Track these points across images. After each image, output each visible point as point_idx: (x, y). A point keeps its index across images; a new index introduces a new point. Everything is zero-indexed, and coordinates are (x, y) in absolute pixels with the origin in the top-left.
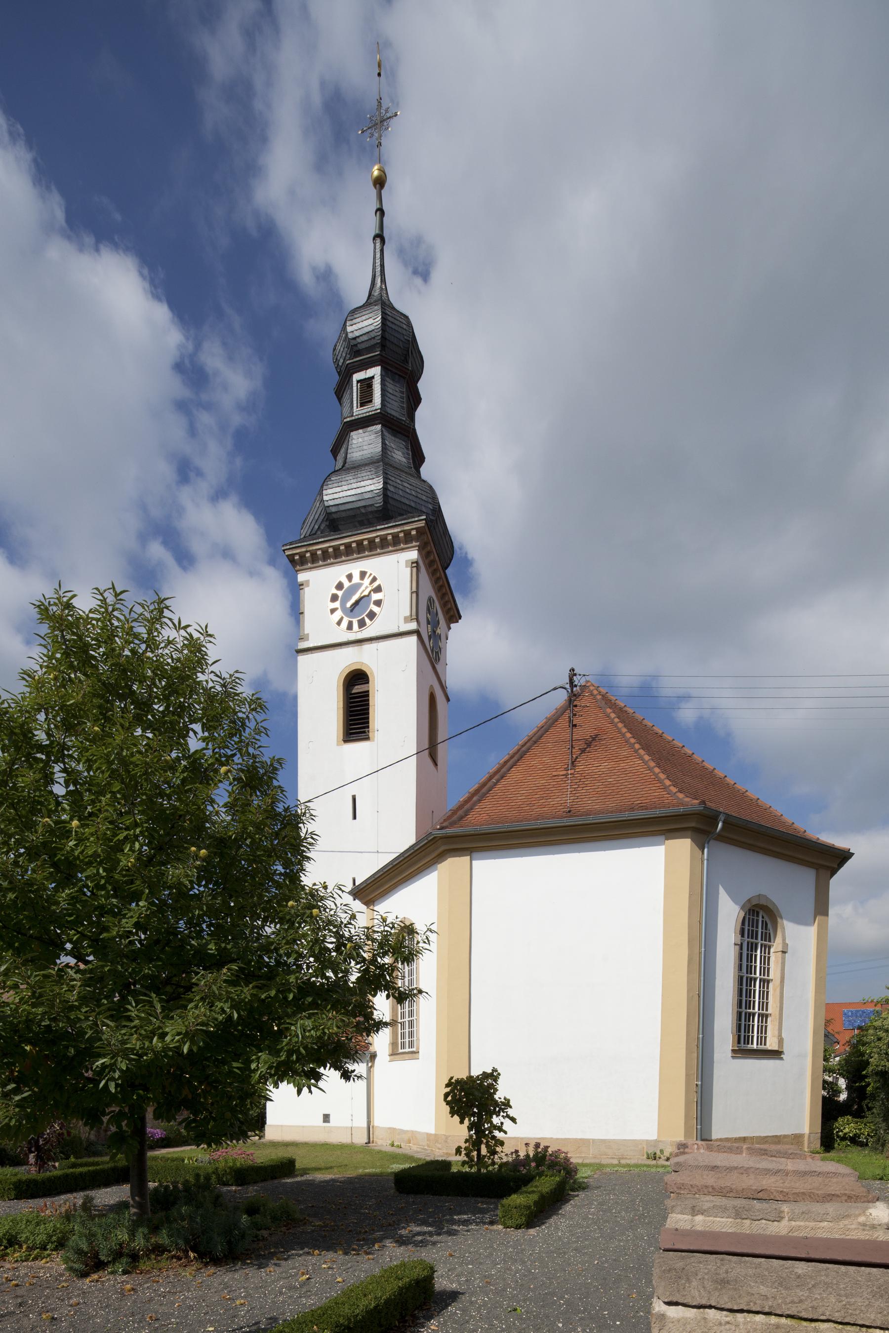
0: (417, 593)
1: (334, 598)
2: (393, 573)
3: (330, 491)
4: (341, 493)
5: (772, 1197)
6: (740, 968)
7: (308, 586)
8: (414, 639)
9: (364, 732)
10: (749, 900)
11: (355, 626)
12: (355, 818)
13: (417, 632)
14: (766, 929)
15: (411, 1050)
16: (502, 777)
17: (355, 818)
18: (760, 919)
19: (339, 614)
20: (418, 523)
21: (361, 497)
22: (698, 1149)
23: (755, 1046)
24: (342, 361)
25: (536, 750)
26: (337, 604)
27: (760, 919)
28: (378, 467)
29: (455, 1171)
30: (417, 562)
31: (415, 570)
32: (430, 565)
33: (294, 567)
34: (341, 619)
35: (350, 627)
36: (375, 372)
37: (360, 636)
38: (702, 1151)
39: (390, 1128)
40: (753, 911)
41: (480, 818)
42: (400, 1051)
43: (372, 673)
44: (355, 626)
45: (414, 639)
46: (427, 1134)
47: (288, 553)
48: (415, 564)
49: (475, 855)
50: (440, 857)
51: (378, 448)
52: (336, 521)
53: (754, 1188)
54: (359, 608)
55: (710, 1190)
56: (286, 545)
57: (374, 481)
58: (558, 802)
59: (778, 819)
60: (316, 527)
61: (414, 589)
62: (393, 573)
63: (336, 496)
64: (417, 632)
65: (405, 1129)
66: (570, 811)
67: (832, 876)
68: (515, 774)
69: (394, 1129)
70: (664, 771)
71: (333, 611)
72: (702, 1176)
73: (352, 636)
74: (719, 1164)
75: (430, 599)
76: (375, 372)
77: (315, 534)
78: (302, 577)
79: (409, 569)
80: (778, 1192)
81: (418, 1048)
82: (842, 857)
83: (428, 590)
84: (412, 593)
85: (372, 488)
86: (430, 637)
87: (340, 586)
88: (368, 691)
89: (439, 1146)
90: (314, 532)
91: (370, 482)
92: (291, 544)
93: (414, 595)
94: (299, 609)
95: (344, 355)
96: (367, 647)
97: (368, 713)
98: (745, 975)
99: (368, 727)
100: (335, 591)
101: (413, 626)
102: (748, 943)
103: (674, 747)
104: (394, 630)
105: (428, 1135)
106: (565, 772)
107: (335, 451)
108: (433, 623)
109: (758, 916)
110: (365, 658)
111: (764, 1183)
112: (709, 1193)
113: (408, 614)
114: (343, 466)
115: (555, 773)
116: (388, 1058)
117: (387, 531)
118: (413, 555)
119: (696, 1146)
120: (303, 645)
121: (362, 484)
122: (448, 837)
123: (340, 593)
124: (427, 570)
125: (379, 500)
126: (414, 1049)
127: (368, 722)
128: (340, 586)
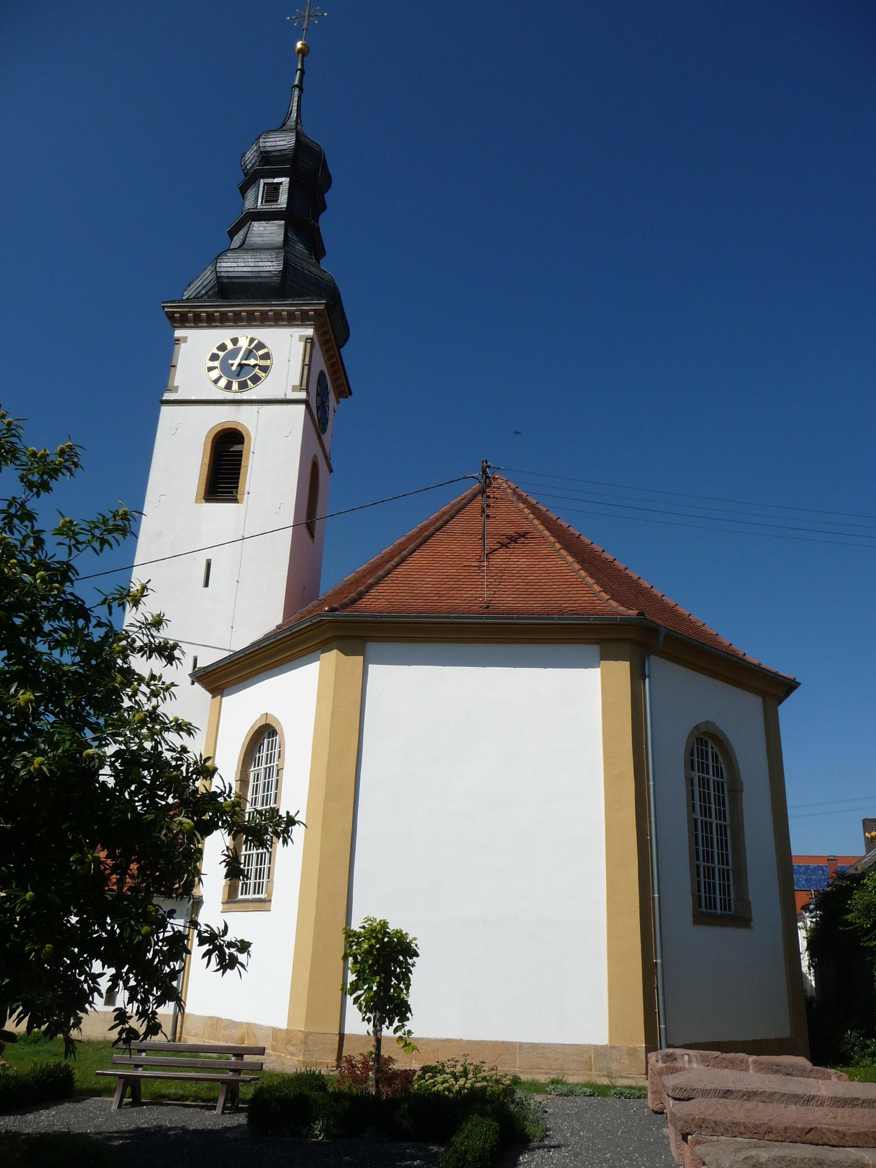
0: (309, 366)
1: (214, 357)
2: (287, 348)
3: (224, 265)
4: (235, 265)
5: (825, 1140)
6: (692, 808)
7: (186, 342)
8: (303, 407)
9: (232, 493)
10: (697, 727)
11: (235, 386)
12: (206, 584)
13: (305, 402)
14: (717, 763)
15: (257, 896)
16: (403, 561)
17: (206, 584)
18: (710, 751)
19: (215, 374)
20: (318, 305)
21: (257, 275)
22: (690, 1062)
23: (719, 911)
24: (250, 165)
25: (439, 536)
26: (216, 363)
27: (710, 751)
28: (279, 253)
29: (241, 1089)
30: (312, 339)
31: (309, 345)
32: (324, 343)
33: (172, 323)
34: (220, 378)
35: (229, 387)
36: (285, 180)
37: (245, 396)
38: (695, 1065)
39: (211, 1018)
40: (701, 739)
41: (377, 602)
42: (240, 897)
43: (249, 434)
44: (235, 386)
45: (303, 407)
46: (274, 1029)
47: (166, 310)
48: (308, 340)
49: (372, 648)
50: (324, 646)
51: (280, 238)
52: (228, 289)
53: (800, 1126)
54: (245, 372)
55: (742, 1130)
56: (167, 302)
57: (274, 264)
58: (475, 595)
59: (698, 630)
60: (203, 292)
61: (307, 362)
62: (287, 348)
63: (229, 269)
64: (305, 402)
65: (236, 1019)
66: (487, 607)
67: (780, 703)
68: (418, 559)
69: (219, 1020)
70: (591, 576)
71: (210, 369)
72: (726, 1106)
73: (229, 396)
74: (731, 1086)
75: (322, 374)
76: (285, 180)
77: (201, 297)
78: (179, 333)
79: (302, 344)
80: (831, 1131)
81: (270, 894)
82: (789, 686)
83: (320, 364)
84: (304, 365)
85: (271, 269)
86: (318, 408)
87: (222, 347)
88: (241, 451)
89: (292, 1049)
90: (199, 295)
91: (270, 264)
92: (173, 302)
93: (306, 368)
94: (171, 362)
95: (253, 161)
96: (245, 408)
97: (239, 474)
98: (700, 819)
99: (237, 488)
100: (216, 352)
101: (303, 395)
102: (699, 778)
103: (592, 551)
104: (281, 396)
105: (275, 1031)
106: (477, 564)
107: (232, 233)
108: (322, 394)
109: (706, 746)
110: (244, 418)
111: (810, 1117)
112: (741, 1134)
113: (298, 383)
114: (239, 247)
115: (465, 564)
116: (221, 907)
117: (284, 307)
118: (310, 332)
119: (686, 1058)
120: (167, 396)
121: (261, 264)
122: (334, 619)
123: (221, 354)
124: (321, 347)
125: (277, 280)
126: (263, 896)
127: (238, 483)
128: (222, 347)
